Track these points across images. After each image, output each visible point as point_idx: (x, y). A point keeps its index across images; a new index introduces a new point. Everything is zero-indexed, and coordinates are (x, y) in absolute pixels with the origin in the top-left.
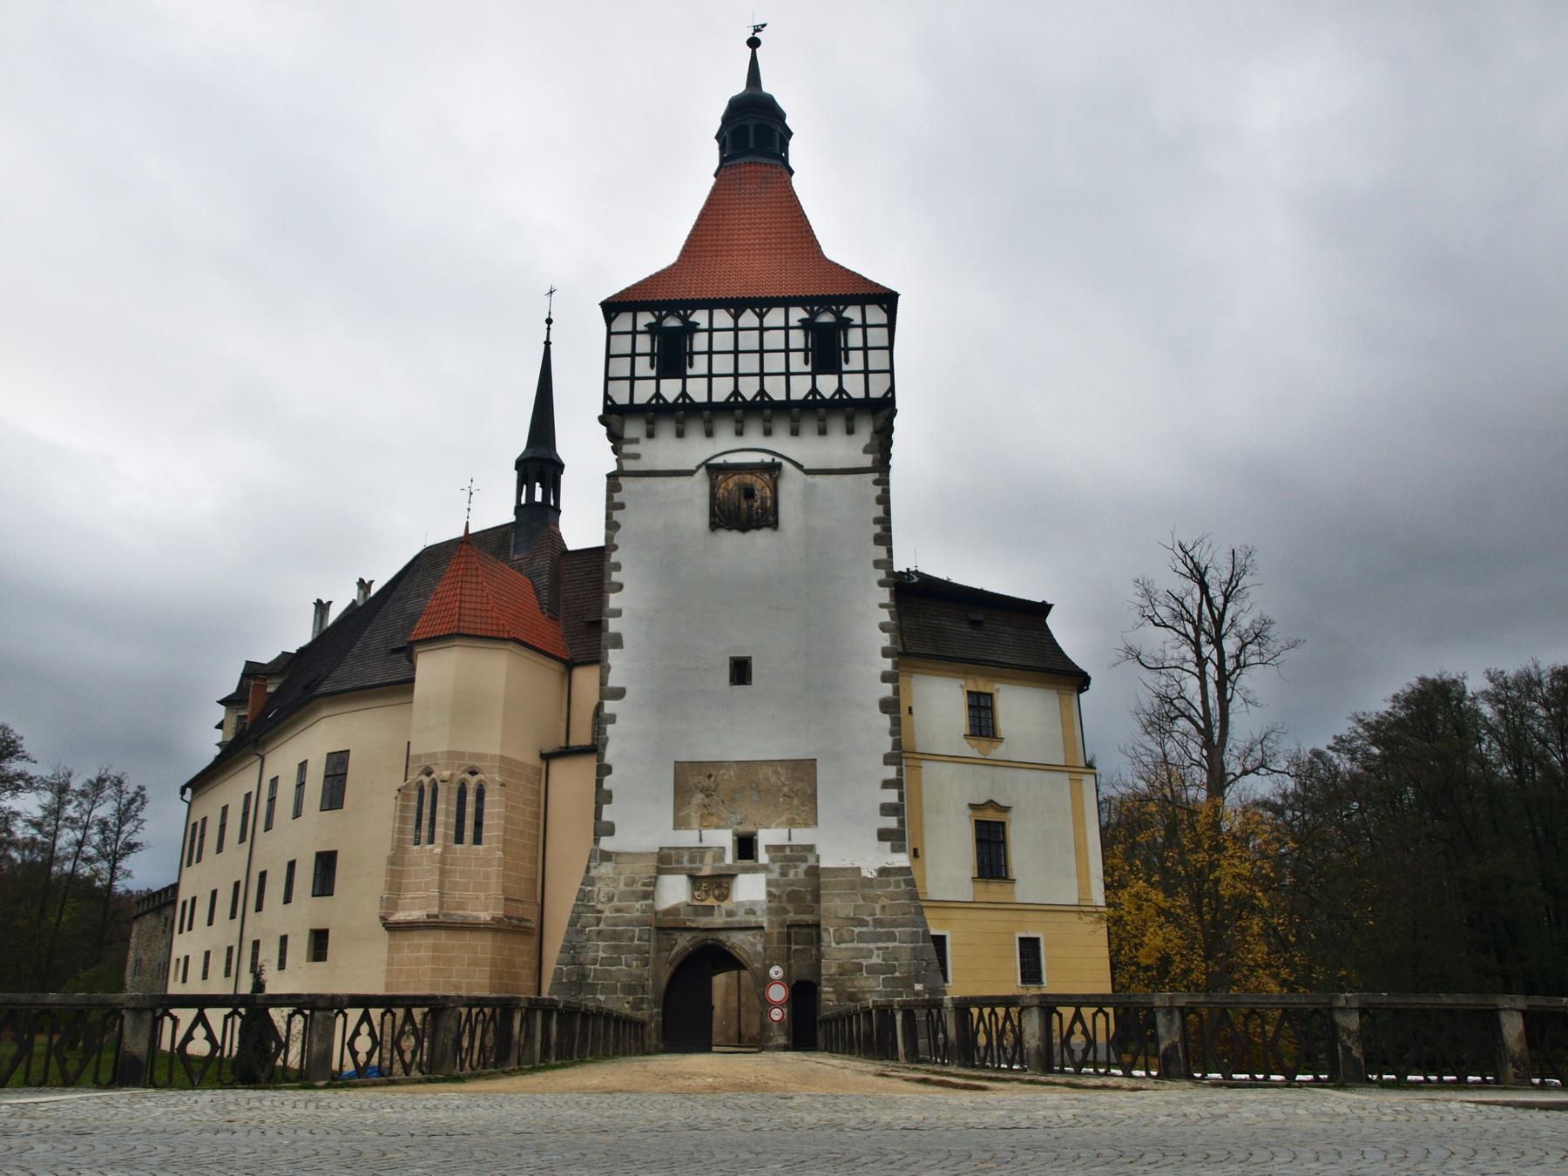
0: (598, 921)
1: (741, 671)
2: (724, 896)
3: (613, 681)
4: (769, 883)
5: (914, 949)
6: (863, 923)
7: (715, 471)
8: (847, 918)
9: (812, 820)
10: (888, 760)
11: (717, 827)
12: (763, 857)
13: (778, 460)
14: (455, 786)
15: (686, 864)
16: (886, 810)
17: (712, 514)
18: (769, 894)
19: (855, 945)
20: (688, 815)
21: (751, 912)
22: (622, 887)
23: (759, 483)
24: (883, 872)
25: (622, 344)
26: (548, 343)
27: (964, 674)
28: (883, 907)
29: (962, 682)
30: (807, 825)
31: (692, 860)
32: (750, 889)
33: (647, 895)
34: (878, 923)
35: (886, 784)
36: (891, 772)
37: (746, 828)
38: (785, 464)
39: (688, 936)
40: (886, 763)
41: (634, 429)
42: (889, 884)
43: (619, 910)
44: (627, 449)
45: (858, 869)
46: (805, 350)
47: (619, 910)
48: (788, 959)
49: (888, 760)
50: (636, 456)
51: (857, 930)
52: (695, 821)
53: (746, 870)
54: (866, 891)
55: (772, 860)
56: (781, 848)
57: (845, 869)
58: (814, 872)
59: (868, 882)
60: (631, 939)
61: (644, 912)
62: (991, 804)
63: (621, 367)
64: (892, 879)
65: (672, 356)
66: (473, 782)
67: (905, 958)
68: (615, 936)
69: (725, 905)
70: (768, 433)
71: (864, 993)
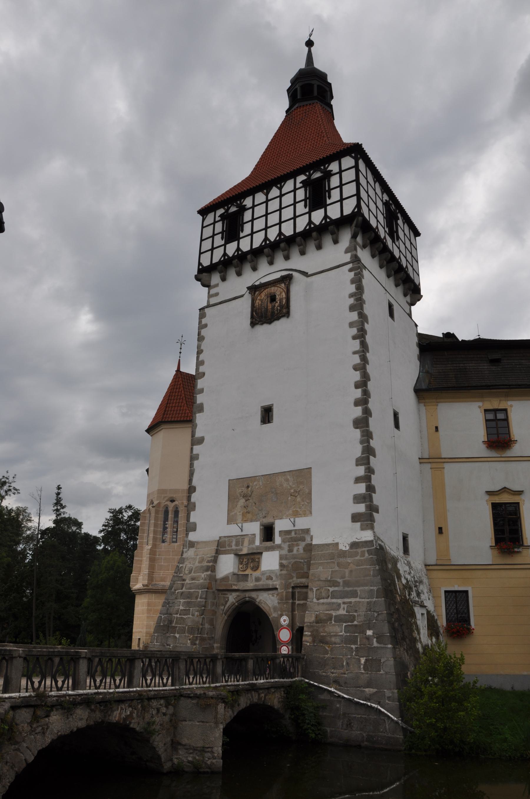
0: (183, 585)
1: (267, 414)
2: (257, 567)
3: (198, 435)
4: (281, 557)
5: (368, 603)
6: (335, 584)
7: (253, 289)
8: (326, 581)
9: (308, 512)
10: (359, 462)
11: (252, 521)
12: (278, 540)
13: (291, 272)
14: (162, 509)
15: (234, 547)
16: (358, 499)
17: (252, 317)
18: (282, 565)
19: (329, 600)
20: (236, 514)
21: (270, 578)
22: (197, 564)
23: (279, 291)
24: (354, 545)
25: (208, 232)
26: (179, 360)
27: (481, 398)
28: (351, 571)
29: (480, 404)
30: (305, 515)
31: (237, 544)
32: (270, 561)
33: (213, 569)
34: (347, 584)
35: (358, 480)
36: (361, 471)
37: (267, 521)
38: (295, 274)
39: (235, 594)
40: (357, 465)
41: (215, 278)
42: (356, 554)
43: (193, 579)
44: (213, 291)
45: (337, 544)
46: (305, 200)
47: (193, 579)
48: (293, 610)
49: (359, 462)
50: (217, 294)
51: (331, 589)
52: (239, 518)
53: (268, 549)
54: (341, 560)
55: (284, 541)
56: (289, 532)
57: (328, 545)
58: (309, 548)
59: (343, 554)
60: (197, 598)
61: (205, 579)
62: (505, 490)
63: (207, 245)
64: (359, 550)
65: (232, 229)
66: (171, 506)
67: (362, 611)
68: (189, 595)
69: (256, 574)
70: (287, 258)
71: (331, 636)
